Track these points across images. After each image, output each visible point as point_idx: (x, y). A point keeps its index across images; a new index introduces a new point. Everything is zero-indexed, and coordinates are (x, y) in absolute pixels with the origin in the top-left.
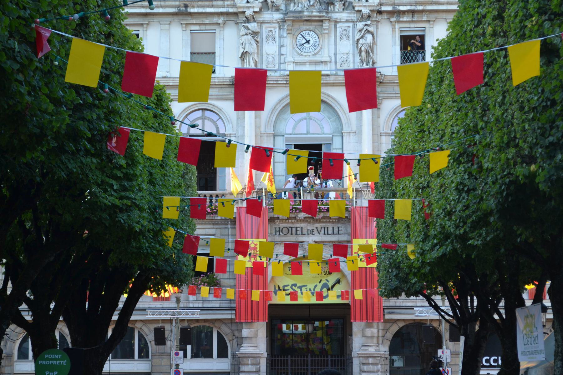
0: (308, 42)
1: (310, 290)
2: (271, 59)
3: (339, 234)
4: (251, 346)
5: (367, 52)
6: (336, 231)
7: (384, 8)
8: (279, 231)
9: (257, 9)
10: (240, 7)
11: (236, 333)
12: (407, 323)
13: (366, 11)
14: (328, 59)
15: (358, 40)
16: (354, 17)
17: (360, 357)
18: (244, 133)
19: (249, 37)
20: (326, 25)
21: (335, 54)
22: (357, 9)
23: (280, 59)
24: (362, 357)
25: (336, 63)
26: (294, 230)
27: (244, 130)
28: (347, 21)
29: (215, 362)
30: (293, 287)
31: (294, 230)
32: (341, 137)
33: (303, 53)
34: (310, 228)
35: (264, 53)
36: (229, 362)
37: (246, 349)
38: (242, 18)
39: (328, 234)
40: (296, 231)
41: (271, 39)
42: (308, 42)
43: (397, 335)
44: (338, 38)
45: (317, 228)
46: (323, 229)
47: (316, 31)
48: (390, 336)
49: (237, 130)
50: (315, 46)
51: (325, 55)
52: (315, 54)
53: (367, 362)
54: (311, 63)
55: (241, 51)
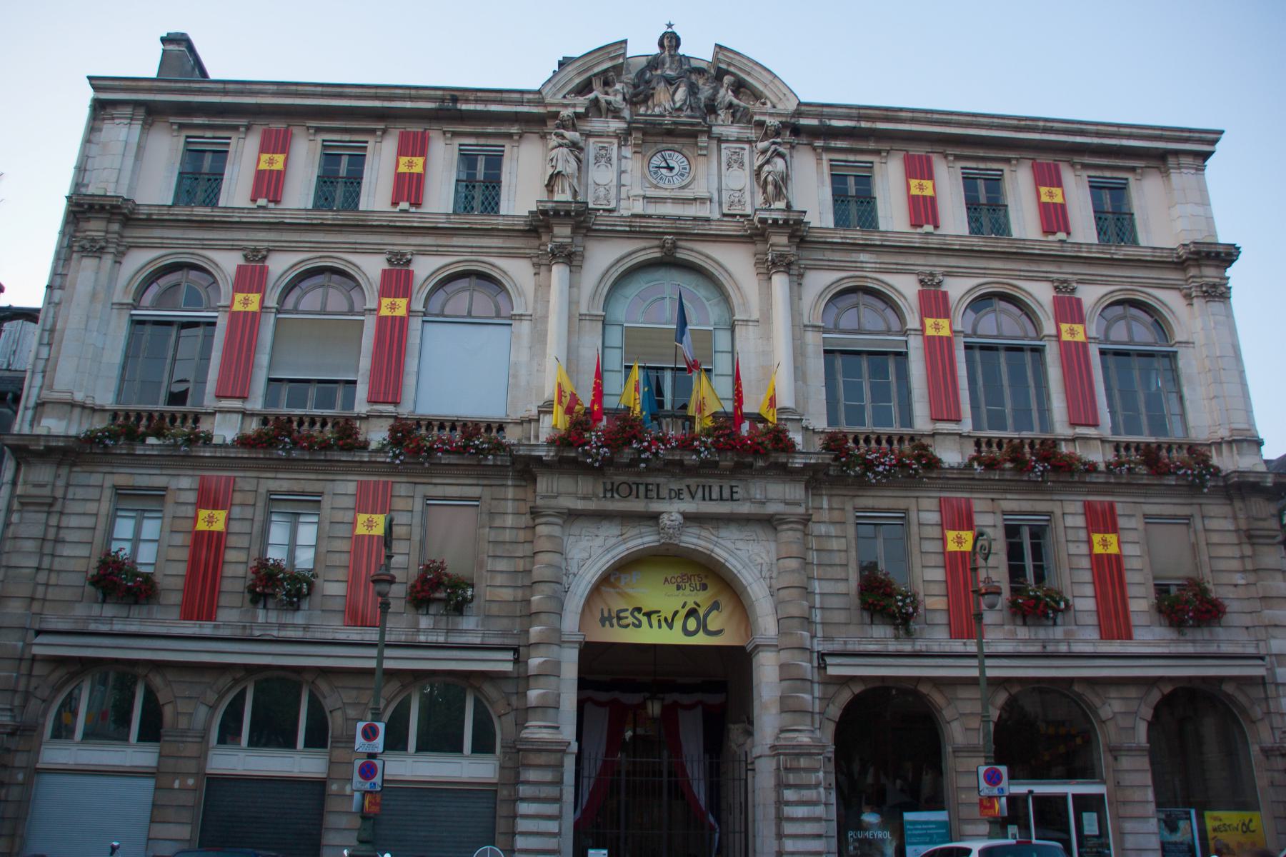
0: (671, 169)
1: (666, 619)
2: (602, 192)
3: (732, 499)
4: (546, 727)
5: (776, 186)
6: (726, 494)
7: (803, 121)
8: (612, 490)
9: (581, 110)
10: (552, 105)
11: (514, 701)
12: (870, 686)
13: (772, 122)
14: (706, 195)
15: (761, 167)
16: (751, 133)
17: (779, 754)
18: (547, 311)
19: (565, 150)
20: (703, 140)
21: (720, 191)
22: (756, 118)
23: (619, 192)
24: (785, 754)
25: (720, 204)
26: (642, 488)
27: (547, 307)
28: (738, 141)
29: (465, 762)
30: (636, 614)
31: (642, 488)
32: (728, 334)
33: (661, 185)
34: (675, 487)
35: (590, 181)
36: (497, 763)
37: (536, 731)
38: (551, 125)
39: (711, 499)
40: (647, 490)
41: (603, 161)
42: (671, 169)
43: (850, 712)
44: (724, 166)
45: (688, 487)
46: (700, 490)
47: (685, 151)
48: (835, 711)
49: (535, 309)
50: (682, 175)
51: (700, 190)
52: (683, 188)
53: (795, 764)
54: (676, 200)
55: (550, 171)
